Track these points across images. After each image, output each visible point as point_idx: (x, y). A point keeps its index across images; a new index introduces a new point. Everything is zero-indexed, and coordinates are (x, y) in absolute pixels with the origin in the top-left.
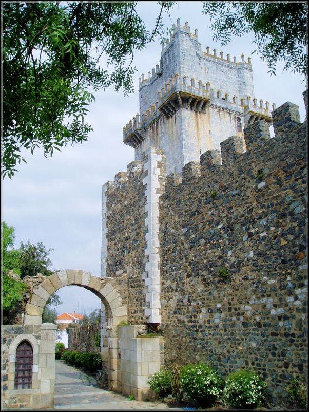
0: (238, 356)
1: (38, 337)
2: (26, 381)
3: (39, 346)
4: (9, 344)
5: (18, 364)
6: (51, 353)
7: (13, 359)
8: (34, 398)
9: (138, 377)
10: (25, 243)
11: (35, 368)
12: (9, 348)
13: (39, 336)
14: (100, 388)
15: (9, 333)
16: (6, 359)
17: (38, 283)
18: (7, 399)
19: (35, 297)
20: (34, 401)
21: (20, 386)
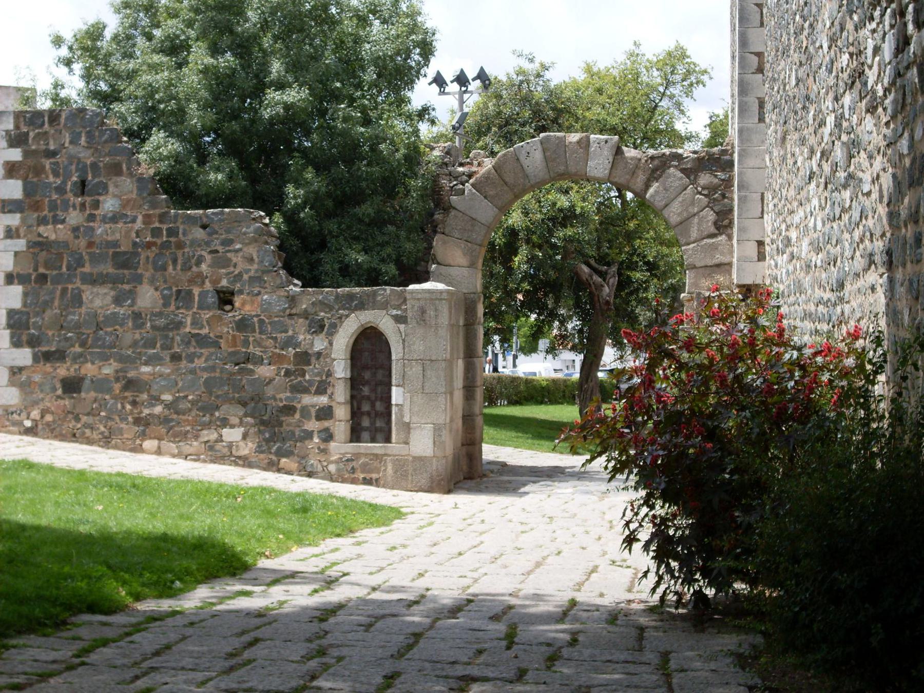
0: (785, 515)
1: (399, 319)
2: (379, 423)
3: (404, 341)
4: (331, 334)
5: (354, 382)
6: (434, 358)
7: (341, 370)
8: (394, 464)
9: (394, 389)
10: (437, 36)
11: (397, 395)
12: (331, 344)
13: (402, 317)
14: (56, 437)
15: (331, 308)
16: (326, 369)
17: (465, 178)
18: (332, 462)
19: (456, 216)
20: (395, 472)
21: (365, 435)
